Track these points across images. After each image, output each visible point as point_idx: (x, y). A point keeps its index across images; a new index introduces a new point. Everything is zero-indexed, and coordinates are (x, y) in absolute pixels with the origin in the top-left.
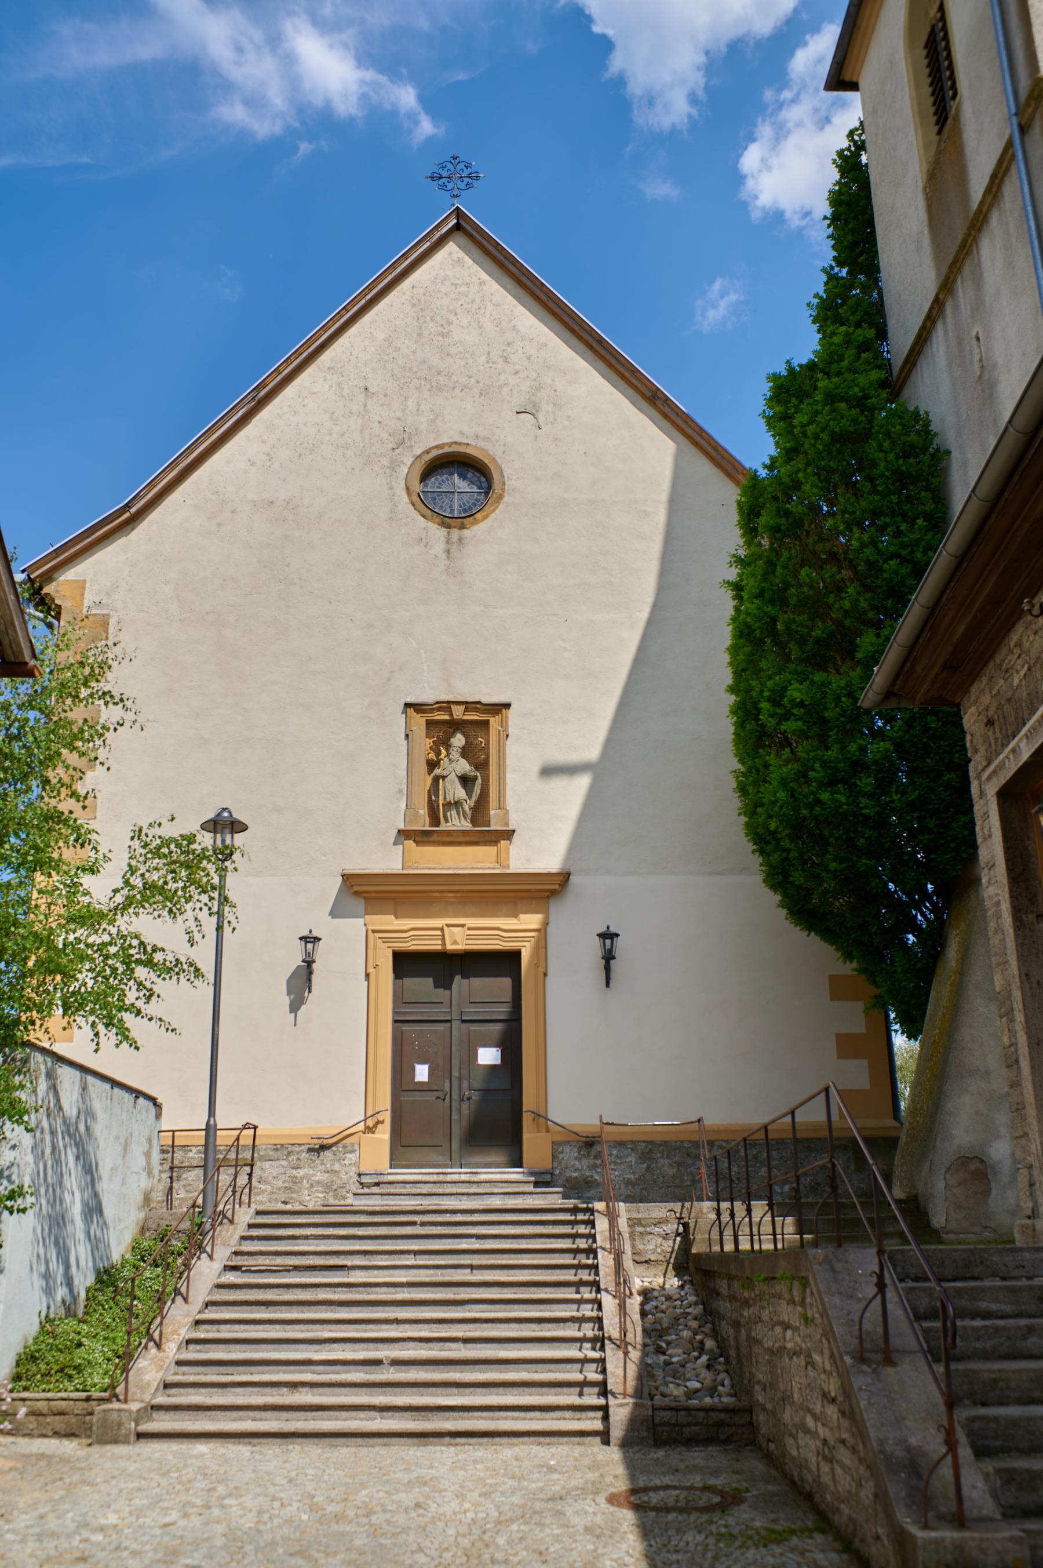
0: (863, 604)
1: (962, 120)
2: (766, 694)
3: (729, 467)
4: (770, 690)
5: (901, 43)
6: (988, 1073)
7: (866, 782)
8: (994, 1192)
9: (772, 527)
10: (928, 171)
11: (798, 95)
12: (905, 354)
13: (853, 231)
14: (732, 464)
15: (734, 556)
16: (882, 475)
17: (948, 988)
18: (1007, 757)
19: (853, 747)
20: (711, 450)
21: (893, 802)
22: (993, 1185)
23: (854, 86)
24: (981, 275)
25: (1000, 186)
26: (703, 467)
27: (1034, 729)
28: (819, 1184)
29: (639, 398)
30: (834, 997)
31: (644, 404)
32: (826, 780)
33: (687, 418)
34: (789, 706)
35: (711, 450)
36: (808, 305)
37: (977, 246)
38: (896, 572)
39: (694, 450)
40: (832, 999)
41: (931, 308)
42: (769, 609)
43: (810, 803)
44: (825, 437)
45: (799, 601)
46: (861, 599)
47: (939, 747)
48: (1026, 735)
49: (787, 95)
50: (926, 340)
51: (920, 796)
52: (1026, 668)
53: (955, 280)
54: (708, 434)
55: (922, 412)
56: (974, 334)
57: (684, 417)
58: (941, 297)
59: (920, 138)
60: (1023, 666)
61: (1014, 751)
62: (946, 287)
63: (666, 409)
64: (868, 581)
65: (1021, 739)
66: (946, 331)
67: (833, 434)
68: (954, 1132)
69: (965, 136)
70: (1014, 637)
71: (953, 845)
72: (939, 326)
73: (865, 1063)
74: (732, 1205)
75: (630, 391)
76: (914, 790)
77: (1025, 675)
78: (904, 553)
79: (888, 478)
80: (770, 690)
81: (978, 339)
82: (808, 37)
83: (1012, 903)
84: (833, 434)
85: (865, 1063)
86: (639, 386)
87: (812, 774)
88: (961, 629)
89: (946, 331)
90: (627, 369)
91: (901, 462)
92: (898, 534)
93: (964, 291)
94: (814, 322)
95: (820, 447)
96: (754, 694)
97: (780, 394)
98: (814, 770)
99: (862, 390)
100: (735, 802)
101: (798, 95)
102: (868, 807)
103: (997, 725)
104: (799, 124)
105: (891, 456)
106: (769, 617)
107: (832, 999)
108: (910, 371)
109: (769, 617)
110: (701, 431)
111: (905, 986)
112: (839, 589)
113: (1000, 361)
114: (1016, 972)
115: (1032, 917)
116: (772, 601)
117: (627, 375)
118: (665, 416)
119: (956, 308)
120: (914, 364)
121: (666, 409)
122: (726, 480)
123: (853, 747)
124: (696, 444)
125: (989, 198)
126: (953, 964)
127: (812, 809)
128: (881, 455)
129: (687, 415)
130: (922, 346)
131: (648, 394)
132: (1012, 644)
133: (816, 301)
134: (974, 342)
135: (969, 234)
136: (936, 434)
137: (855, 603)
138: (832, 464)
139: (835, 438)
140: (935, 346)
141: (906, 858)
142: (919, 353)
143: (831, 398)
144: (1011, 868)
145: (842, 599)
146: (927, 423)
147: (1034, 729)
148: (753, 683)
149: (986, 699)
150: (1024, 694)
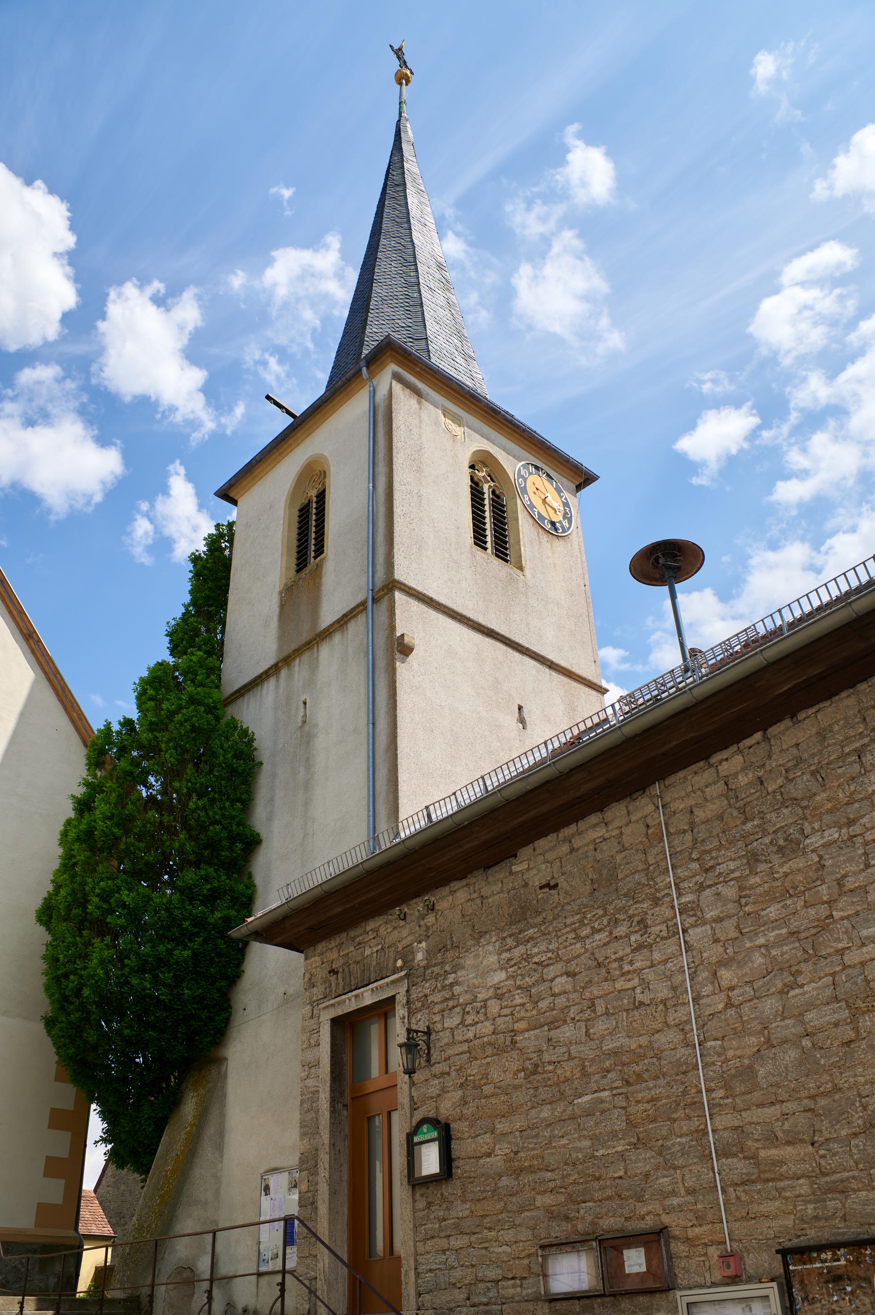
0: (188, 848)
1: (324, 569)
2: (97, 891)
3: (69, 705)
4: (101, 889)
5: (284, 499)
6: (206, 1204)
7: (166, 976)
8: (196, 1296)
9: (127, 771)
10: (286, 584)
11: (17, 396)
12: (235, 689)
13: (210, 589)
14: (72, 703)
15: (84, 779)
16: (220, 765)
17: (183, 1136)
18: (349, 999)
19: (162, 948)
20: (60, 692)
21: (183, 994)
22: (196, 1290)
23: (234, 502)
24: (317, 667)
25: (346, 623)
26: (49, 698)
27: (381, 987)
28: (8, 1282)
29: (17, 631)
30: (52, 1125)
31: (20, 637)
32: (136, 968)
33: (49, 660)
34: (114, 905)
35: (59, 688)
36: (168, 623)
37: (318, 651)
38: (217, 834)
39: (47, 683)
40: (49, 1128)
41: (269, 669)
42: (115, 830)
43: (120, 983)
44: (188, 726)
45: (140, 831)
46: (187, 844)
47: (220, 962)
48: (372, 990)
49: (9, 392)
50: (257, 685)
51: (201, 993)
52: (380, 947)
53: (294, 659)
54: (61, 676)
55: (250, 732)
56: (303, 699)
57: (47, 658)
58: (280, 665)
59: (284, 561)
60: (377, 945)
61: (356, 996)
62: (285, 661)
63: (36, 648)
64: (194, 833)
65: (367, 991)
66: (277, 687)
67: (193, 726)
68: (178, 1247)
69: (324, 580)
70: (371, 925)
71: (212, 1032)
72: (272, 681)
73: (62, 1182)
74: (23, 1299)
75: (13, 624)
76: (198, 989)
77: (377, 951)
78: (224, 822)
79: (223, 768)
80: (101, 889)
81: (305, 703)
82: (37, 363)
83: (331, 1094)
84: (193, 726)
85: (62, 1182)
86: (21, 624)
87: (126, 961)
88: (339, 909)
89: (277, 687)
90: (16, 609)
91: (234, 761)
92: (223, 808)
93: (299, 669)
94: (167, 635)
95: (183, 732)
96: (87, 888)
97: (154, 682)
98: (130, 959)
99: (214, 702)
100: (42, 966)
101: (17, 396)
102: (163, 994)
103: (340, 975)
104: (10, 416)
105: (229, 756)
106: (114, 836)
107: (49, 1128)
108: (238, 698)
109: (114, 836)
110: (57, 672)
111: (145, 1129)
112: (172, 832)
113: (321, 724)
114: (327, 1142)
115: (340, 1106)
116: (118, 825)
117: (15, 613)
118: (33, 652)
119: (290, 677)
120: (242, 695)
121: (36, 648)
122: (64, 713)
123: (162, 948)
124: (49, 680)
125: (336, 626)
126: (190, 1118)
127: (121, 987)
128: (221, 752)
129: (50, 658)
130: (253, 687)
131: (25, 631)
132: (368, 929)
133: (173, 623)
134: (302, 705)
135: (315, 639)
136: (256, 749)
137: (182, 846)
138: (188, 746)
139: (194, 729)
140: (264, 692)
141: (179, 1035)
142: (249, 690)
143: (193, 700)
144: (333, 1071)
145: (174, 840)
146: (252, 740)
147: (381, 987)
148: (89, 880)
149: (333, 955)
150: (374, 963)
